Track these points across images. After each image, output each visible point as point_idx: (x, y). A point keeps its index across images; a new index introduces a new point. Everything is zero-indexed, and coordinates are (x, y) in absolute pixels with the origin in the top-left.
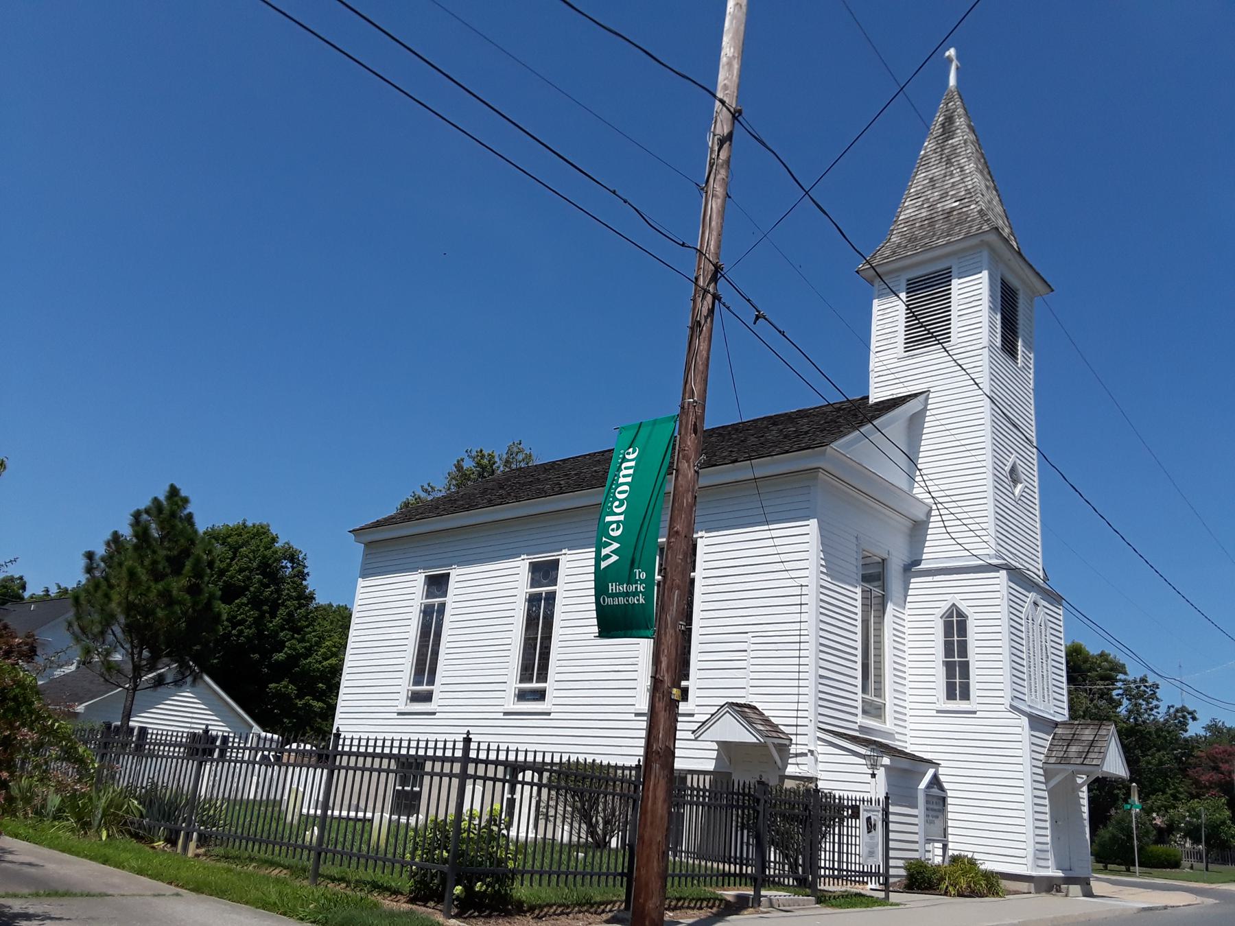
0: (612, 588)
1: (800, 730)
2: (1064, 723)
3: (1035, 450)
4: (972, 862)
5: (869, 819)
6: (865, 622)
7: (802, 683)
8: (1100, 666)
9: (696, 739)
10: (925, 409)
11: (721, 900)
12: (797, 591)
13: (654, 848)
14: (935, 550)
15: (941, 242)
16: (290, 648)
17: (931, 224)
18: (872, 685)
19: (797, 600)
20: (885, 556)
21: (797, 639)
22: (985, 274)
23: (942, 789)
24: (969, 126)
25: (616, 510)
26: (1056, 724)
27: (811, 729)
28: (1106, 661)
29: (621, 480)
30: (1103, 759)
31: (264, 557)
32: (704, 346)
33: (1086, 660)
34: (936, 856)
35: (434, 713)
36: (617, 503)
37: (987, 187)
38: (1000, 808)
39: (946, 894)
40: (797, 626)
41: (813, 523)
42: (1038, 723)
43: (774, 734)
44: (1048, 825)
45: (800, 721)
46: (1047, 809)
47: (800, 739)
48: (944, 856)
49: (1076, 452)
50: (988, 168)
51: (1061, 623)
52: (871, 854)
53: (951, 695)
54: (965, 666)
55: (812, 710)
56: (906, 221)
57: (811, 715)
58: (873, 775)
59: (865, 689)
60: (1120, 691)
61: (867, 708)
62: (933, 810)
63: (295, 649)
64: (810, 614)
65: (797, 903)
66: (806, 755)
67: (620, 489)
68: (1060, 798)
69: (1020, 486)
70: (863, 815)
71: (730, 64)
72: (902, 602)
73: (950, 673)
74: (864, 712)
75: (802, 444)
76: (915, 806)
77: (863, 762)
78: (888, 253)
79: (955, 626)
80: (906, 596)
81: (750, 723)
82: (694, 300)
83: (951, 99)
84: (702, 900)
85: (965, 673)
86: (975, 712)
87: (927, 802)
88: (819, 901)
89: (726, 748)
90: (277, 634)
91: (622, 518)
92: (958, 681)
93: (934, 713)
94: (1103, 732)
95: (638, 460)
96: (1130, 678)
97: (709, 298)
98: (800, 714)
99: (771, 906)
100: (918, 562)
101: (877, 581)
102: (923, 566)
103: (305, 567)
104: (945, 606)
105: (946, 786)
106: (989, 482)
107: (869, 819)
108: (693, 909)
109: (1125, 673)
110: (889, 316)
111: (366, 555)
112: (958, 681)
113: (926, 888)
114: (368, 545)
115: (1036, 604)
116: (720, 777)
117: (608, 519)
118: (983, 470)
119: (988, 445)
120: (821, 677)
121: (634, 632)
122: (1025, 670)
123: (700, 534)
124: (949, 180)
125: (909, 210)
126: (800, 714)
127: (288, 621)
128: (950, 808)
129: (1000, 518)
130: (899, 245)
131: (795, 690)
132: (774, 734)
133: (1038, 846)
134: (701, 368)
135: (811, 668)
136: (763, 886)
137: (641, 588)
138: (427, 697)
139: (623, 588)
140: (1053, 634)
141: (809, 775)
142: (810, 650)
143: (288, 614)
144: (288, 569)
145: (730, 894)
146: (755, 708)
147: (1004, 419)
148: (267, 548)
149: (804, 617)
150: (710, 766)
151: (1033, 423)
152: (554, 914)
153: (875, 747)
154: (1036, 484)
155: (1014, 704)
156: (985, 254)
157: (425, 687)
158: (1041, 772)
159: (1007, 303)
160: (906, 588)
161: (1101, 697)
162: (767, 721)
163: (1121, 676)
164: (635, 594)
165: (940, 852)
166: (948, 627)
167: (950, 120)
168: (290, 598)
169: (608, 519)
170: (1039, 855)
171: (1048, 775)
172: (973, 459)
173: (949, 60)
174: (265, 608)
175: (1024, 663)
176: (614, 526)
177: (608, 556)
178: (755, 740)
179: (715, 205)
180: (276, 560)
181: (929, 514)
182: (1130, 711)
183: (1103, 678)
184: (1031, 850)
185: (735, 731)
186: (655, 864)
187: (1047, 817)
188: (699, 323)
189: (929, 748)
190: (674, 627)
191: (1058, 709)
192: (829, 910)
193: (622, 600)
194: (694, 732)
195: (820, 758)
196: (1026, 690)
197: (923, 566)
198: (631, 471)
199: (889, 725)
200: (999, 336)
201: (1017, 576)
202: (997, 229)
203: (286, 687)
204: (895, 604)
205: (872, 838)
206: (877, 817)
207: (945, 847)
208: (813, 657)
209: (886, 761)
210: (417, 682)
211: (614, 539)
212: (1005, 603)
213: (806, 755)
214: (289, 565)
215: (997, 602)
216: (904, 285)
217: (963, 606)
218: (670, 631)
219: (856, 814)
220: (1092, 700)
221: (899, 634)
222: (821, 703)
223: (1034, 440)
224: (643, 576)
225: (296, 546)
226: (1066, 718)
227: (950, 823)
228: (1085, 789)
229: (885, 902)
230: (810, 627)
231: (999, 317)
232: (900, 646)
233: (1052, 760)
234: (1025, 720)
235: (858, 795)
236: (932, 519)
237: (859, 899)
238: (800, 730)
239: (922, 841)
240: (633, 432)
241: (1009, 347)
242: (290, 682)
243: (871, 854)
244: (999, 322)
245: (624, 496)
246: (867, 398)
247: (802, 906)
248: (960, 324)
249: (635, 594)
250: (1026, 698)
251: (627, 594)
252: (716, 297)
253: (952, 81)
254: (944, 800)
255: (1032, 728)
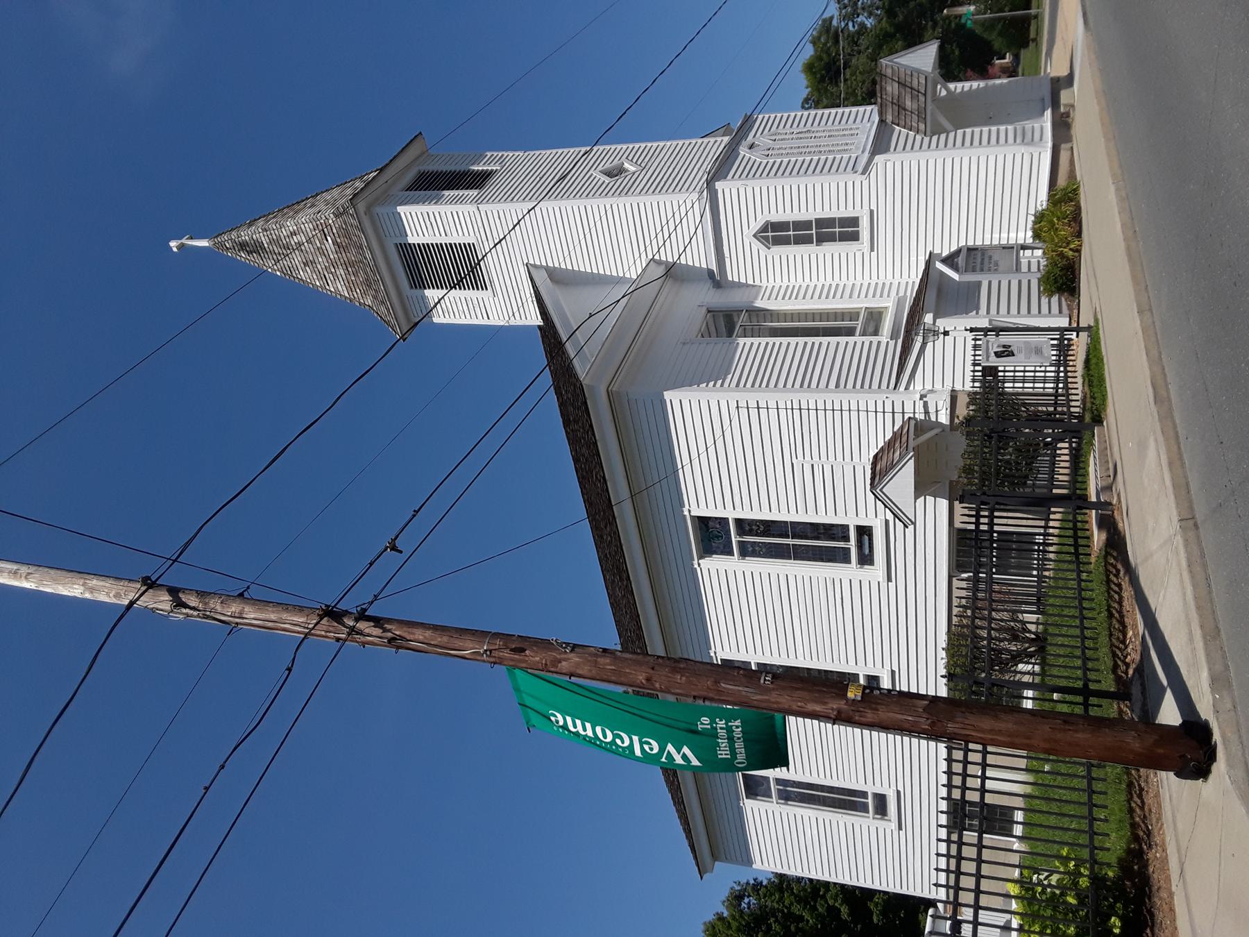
0: (724, 754)
1: (898, 409)
2: (881, 113)
3: (595, 149)
4: (1040, 217)
5: (998, 355)
6: (776, 333)
7: (845, 407)
8: (825, 44)
9: (914, 524)
10: (547, 268)
11: (1107, 554)
12: (744, 412)
13: (1059, 736)
14: (700, 257)
15: (369, 255)
16: (836, 900)
17: (352, 264)
18: (846, 323)
19: (754, 412)
20: (704, 310)
21: (797, 412)
22: (400, 209)
23: (959, 251)
24: (250, 225)
25: (627, 743)
26: (882, 121)
27: (898, 398)
28: (819, 38)
29: (590, 733)
30: (919, 72)
31: (739, 930)
32: (419, 634)
33: (820, 58)
34: (1035, 257)
35: (898, 792)
36: (618, 741)
37: (313, 206)
38: (972, 186)
39: (1078, 251)
40: (783, 412)
41: (668, 395)
42: (881, 144)
43: (904, 439)
44: (994, 129)
45: (889, 408)
46: (977, 130)
47: (909, 408)
48: (1033, 248)
49: (597, 106)
50: (293, 205)
51: (779, 115)
52: (1038, 351)
53: (855, 237)
54: (821, 223)
55: (876, 396)
56: (350, 289)
57: (880, 398)
58: (946, 333)
59: (850, 332)
60: (850, 24)
61: (871, 329)
62: (982, 263)
63: (837, 895)
64: (769, 398)
65: (1103, 451)
66: (926, 404)
67: (601, 737)
68: (961, 116)
69: (626, 165)
70: (993, 361)
71: (92, 590)
72: (754, 290)
73: (831, 238)
74: (876, 333)
75: (587, 404)
76: (979, 284)
77: (930, 345)
78: (383, 308)
79: (777, 234)
80: (747, 285)
81: (893, 466)
82: (364, 644)
83: (222, 244)
84: (1108, 581)
85: (830, 222)
86: (872, 212)
87: (974, 270)
88: (1098, 420)
89: (922, 487)
90: (820, 915)
91: (635, 738)
92: (842, 230)
93: (874, 254)
94: (889, 72)
95: (564, 713)
96: (836, 14)
97: (362, 625)
98: (880, 409)
99: (1109, 488)
100: (710, 273)
101: (733, 320)
102: (714, 267)
103: (748, 883)
104: (757, 245)
105: (954, 248)
106: (622, 201)
107: (998, 355)
108: (1121, 598)
109: (832, 18)
110: (453, 307)
111: (727, 860)
112: (842, 230)
113: (1073, 273)
114: (715, 857)
115: (751, 147)
116: (956, 495)
117: (638, 752)
118: (615, 207)
119: (582, 203)
120: (837, 386)
121: (779, 730)
122: (823, 158)
123: (686, 513)
124: (304, 244)
125: (338, 287)
126: (880, 409)
127: (807, 903)
128: (979, 243)
129: (660, 189)
130: (375, 297)
131: (854, 414)
132: (904, 439)
133: (1018, 141)
134: (445, 639)
135: (829, 397)
136: (1084, 498)
137: (722, 724)
138: (881, 801)
139: (723, 743)
140: (790, 124)
141: (948, 400)
142: (808, 399)
143: (799, 902)
144: (749, 902)
145: (1098, 538)
146: (876, 457)
147: (560, 186)
148: (729, 927)
149: (772, 404)
150: (943, 504)
151: (560, 151)
152: (1142, 808)
153: (912, 328)
154: (625, 147)
155: (860, 170)
156: (379, 210)
157: (870, 801)
158: (935, 138)
159: (433, 183)
160: (739, 285)
161: (856, 43)
162: (890, 445)
163: (835, 23)
164: (729, 730)
165: (1028, 253)
166: (778, 241)
167: (243, 246)
168: (781, 900)
169: (638, 752)
170: (1026, 139)
171: (937, 130)
172: (597, 218)
173: (181, 247)
174: (793, 928)
175: (816, 158)
176: (646, 747)
177: (684, 757)
178: (912, 461)
179: (252, 614)
180: (741, 917)
181: (659, 263)
182: (870, 14)
183: (837, 41)
184: (1023, 149)
185: (903, 481)
186: (1080, 735)
187: (985, 129)
188: (391, 640)
189: (913, 259)
190: (765, 690)
191: (865, 118)
192: (1110, 409)
193: (739, 745)
194: (906, 526)
195: (929, 387)
196: (846, 156)
197: (714, 267)
198: (578, 722)
199: (889, 304)
200: (466, 192)
201: (722, 168)
202: (355, 195)
203: (876, 905)
204: (756, 298)
205: (1020, 352)
206: (995, 343)
207: (1024, 247)
208: (816, 396)
209: (928, 318)
210: (864, 808)
211: (662, 749)
212: (750, 183)
213: (926, 404)
214: (746, 900)
215: (749, 190)
216: (417, 292)
217: (756, 226)
218: (773, 697)
219: (990, 371)
220: (859, 52)
221: (789, 293)
222: (867, 385)
223: (583, 150)
224: (705, 720)
225: (725, 893)
226: (875, 108)
227: (995, 242)
228: (952, 86)
229: (1093, 331)
230: (783, 399)
231: (446, 193)
232: (802, 305)
233: (922, 126)
234: (879, 159)
235: (969, 368)
236: (663, 258)
237: (1093, 361)
238: (898, 409)
239: (1019, 276)
240: (532, 714)
241: (477, 181)
242: (871, 900)
243: (1038, 351)
244: (452, 193)
245: (608, 732)
246: (539, 327)
247: (1101, 436)
248: (455, 234)
249: (729, 730)
250: (854, 156)
251: (731, 739)
252: (362, 616)
253: (204, 243)
254: (971, 250)
255: (886, 150)
